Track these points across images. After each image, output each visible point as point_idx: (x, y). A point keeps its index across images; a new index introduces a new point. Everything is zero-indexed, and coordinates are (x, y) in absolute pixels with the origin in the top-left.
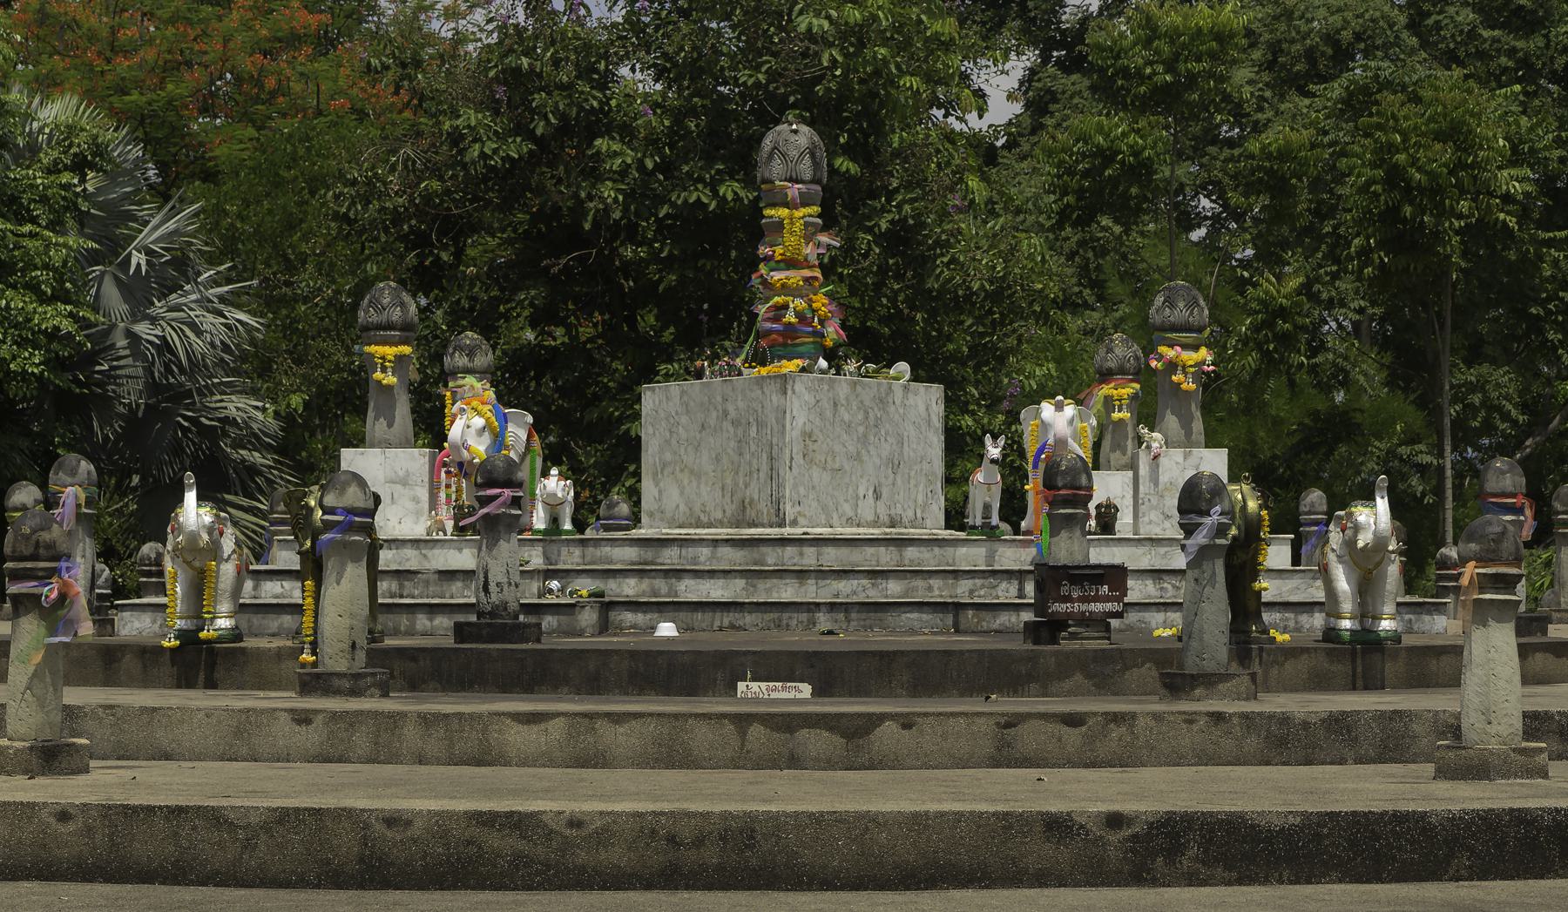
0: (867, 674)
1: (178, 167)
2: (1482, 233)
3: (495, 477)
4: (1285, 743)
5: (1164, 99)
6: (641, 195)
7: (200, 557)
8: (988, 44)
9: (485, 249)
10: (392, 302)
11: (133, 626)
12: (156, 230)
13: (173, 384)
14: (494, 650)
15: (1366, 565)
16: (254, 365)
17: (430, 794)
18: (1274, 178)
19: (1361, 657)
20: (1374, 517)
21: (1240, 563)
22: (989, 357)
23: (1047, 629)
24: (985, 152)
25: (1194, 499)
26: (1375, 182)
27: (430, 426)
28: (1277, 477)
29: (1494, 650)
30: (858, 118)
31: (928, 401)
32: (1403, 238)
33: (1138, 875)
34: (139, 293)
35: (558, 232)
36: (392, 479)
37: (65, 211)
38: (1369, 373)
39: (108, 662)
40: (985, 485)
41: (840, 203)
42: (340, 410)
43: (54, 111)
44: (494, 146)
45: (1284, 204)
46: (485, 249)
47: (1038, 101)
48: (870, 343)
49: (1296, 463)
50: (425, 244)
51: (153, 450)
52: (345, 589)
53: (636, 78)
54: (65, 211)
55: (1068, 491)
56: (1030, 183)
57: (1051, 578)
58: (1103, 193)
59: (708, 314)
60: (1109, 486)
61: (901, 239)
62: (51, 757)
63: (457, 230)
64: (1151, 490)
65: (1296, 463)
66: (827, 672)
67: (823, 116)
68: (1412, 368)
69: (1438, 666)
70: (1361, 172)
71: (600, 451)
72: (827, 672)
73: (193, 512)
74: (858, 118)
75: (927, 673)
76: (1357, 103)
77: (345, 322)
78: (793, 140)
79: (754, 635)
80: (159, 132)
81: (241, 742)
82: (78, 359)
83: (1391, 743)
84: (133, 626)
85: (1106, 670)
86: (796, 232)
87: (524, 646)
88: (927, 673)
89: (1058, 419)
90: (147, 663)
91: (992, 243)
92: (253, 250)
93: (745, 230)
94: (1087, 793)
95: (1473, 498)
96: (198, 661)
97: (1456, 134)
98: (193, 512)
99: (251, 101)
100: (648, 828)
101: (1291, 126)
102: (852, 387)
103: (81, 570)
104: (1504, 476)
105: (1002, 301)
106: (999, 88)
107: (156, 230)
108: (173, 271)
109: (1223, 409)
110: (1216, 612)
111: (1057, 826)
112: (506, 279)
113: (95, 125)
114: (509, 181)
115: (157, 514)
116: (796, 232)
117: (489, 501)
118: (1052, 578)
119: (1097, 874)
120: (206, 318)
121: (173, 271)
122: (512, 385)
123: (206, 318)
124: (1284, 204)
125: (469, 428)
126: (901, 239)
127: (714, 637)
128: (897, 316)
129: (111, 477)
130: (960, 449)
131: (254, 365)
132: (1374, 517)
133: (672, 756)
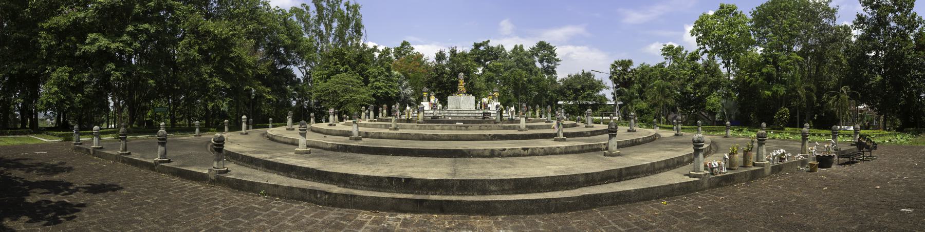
0: (468, 122)
1: (407, 77)
2: (523, 84)
3: (435, 104)
4: (505, 128)
5: (495, 71)
6: (448, 80)
7: (408, 112)
8: (479, 66)
9: (434, 84)
10: (425, 89)
11: (403, 118)
12: (405, 83)
13: (406, 97)
14: (435, 120)
15: (512, 113)
16: (413, 95)
17: (429, 132)
18: (504, 79)
19: (512, 121)
20: (513, 109)
21: (501, 113)
22: (479, 94)
23: (484, 118)
24: (479, 76)
25: (497, 107)
26: (120, 64)
27: (429, 100)
28: (505, 105)
29: (523, 120)
30: (467, 73)
31: (474, 98)
32: (516, 84)
33: (492, 140)
34: (403, 89)
35: (441, 83)
36: (426, 105)
37: (397, 81)
38: (513, 96)
39: (401, 121)
40: (478, 105)
41: (466, 80)
42: (421, 99)
43: (396, 73)
44: (435, 75)
45: (505, 81)
46: (434, 84)
47: (484, 71)
48: (468, 93)
49: (506, 104)
50: (428, 84)
51: (405, 102)
52: (421, 114)
53: (447, 69)
54: (397, 81)
55: (486, 106)
56: (483, 79)
57: (484, 114)
58: (489, 80)
59: (454, 90)
60: (489, 106)
61: (471, 84)
62: (396, 129)
63: (431, 83)
64: (493, 106)
65: (506, 104)
66: (464, 122)
67: (464, 72)
68: (516, 96)
69: (518, 121)
70: (512, 78)
71: (444, 102)
72: (464, 122)
73: (408, 108)
74: (467, 73)
75: (473, 122)
76: (512, 72)
77: (421, 91)
78: (462, 74)
79: (458, 119)
80: (405, 75)
81: (412, 128)
82: (398, 94)
83: (514, 128)
84: (403, 118)
85: (489, 122)
86: (462, 83)
87: (410, 196)
88: (473, 122)
89: (485, 100)
90: (404, 121)
91: (478, 84)
92: (413, 85)
93: (458, 82)
94: (487, 132)
95: (521, 107)
96: (409, 121)
97: (520, 75)
98: (408, 108)
99: (413, 71)
100: (448, 135)
101: (506, 74)
102: (467, 97)
103: (398, 112)
104: (524, 105)
105: (480, 89)
106: (480, 70)
107: (405, 83)
108: (406, 87)
109: (500, 99)
110: (499, 117)
111: (485, 135)
112: (436, 87)
113: (400, 74)
114: (436, 78)
115: (405, 109)
116: (462, 83)
117: (434, 107)
118: (484, 114)
119: (488, 140)
120: (409, 91)
121: (406, 87)
122: (436, 96)
123: (409, 91)
124: (505, 81)
125: (433, 99)
126: (471, 84)
127: (454, 119)
128: (471, 90)
129: (401, 105)
130: (476, 102)
131: (413, 95)
132: (513, 109)
133: (451, 129)
